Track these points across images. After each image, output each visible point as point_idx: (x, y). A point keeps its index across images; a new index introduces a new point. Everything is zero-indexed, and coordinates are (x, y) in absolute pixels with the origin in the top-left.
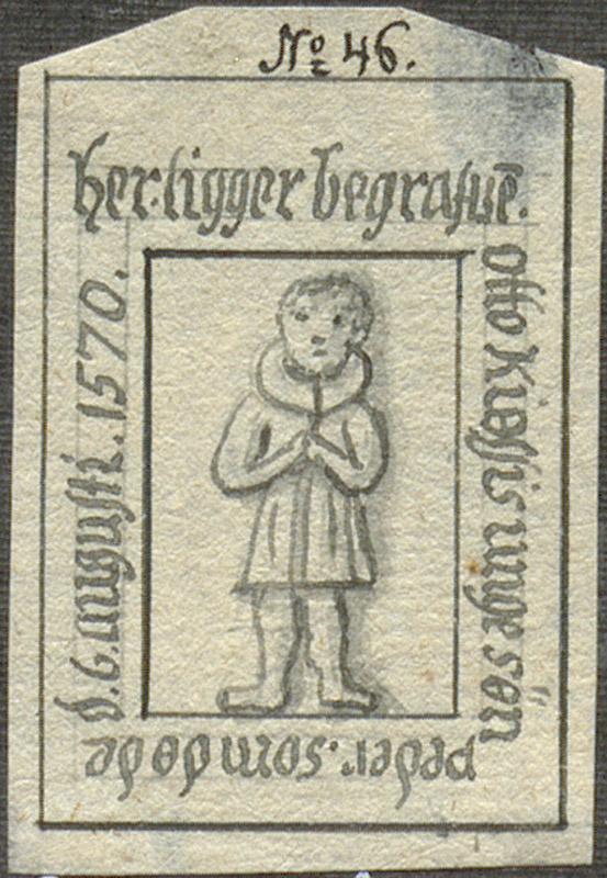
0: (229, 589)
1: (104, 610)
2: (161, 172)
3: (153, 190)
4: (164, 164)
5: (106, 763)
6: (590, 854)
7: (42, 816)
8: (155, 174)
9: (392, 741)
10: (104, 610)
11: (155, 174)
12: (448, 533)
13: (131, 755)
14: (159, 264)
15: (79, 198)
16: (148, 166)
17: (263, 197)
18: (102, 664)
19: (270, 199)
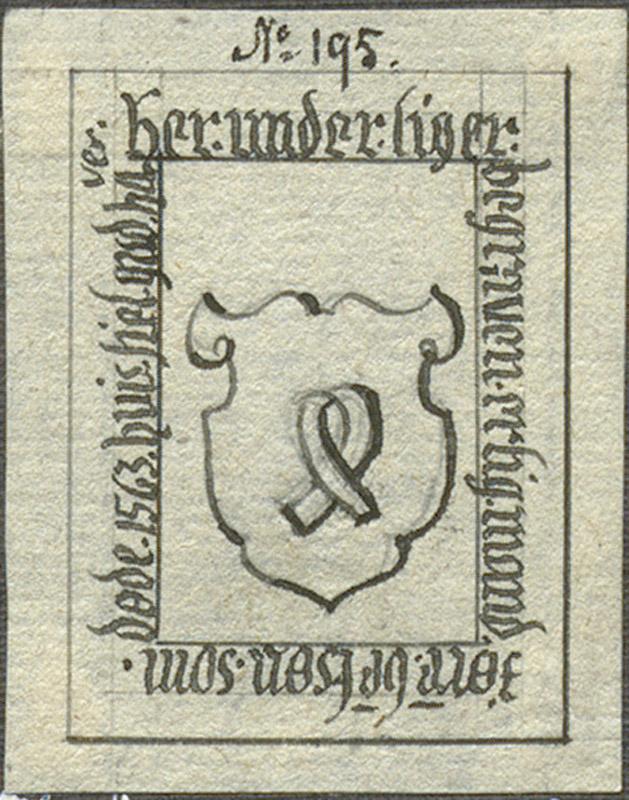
0: (516, 702)
1: (496, 538)
2: (386, 117)
3: (382, 135)
4: (388, 109)
5: (167, 124)
6: (612, 12)
7: (69, 731)
8: (380, 121)
9: (500, 654)
10: (496, 538)
11: (380, 121)
12: (554, 205)
13: (310, 134)
14: (556, 730)
15: (132, 142)
16: (373, 112)
17: (499, 337)
18: (185, 133)
19: (499, 343)
